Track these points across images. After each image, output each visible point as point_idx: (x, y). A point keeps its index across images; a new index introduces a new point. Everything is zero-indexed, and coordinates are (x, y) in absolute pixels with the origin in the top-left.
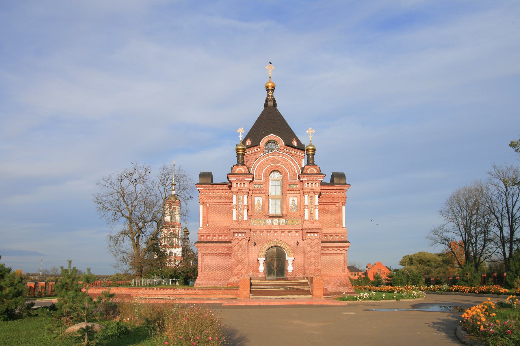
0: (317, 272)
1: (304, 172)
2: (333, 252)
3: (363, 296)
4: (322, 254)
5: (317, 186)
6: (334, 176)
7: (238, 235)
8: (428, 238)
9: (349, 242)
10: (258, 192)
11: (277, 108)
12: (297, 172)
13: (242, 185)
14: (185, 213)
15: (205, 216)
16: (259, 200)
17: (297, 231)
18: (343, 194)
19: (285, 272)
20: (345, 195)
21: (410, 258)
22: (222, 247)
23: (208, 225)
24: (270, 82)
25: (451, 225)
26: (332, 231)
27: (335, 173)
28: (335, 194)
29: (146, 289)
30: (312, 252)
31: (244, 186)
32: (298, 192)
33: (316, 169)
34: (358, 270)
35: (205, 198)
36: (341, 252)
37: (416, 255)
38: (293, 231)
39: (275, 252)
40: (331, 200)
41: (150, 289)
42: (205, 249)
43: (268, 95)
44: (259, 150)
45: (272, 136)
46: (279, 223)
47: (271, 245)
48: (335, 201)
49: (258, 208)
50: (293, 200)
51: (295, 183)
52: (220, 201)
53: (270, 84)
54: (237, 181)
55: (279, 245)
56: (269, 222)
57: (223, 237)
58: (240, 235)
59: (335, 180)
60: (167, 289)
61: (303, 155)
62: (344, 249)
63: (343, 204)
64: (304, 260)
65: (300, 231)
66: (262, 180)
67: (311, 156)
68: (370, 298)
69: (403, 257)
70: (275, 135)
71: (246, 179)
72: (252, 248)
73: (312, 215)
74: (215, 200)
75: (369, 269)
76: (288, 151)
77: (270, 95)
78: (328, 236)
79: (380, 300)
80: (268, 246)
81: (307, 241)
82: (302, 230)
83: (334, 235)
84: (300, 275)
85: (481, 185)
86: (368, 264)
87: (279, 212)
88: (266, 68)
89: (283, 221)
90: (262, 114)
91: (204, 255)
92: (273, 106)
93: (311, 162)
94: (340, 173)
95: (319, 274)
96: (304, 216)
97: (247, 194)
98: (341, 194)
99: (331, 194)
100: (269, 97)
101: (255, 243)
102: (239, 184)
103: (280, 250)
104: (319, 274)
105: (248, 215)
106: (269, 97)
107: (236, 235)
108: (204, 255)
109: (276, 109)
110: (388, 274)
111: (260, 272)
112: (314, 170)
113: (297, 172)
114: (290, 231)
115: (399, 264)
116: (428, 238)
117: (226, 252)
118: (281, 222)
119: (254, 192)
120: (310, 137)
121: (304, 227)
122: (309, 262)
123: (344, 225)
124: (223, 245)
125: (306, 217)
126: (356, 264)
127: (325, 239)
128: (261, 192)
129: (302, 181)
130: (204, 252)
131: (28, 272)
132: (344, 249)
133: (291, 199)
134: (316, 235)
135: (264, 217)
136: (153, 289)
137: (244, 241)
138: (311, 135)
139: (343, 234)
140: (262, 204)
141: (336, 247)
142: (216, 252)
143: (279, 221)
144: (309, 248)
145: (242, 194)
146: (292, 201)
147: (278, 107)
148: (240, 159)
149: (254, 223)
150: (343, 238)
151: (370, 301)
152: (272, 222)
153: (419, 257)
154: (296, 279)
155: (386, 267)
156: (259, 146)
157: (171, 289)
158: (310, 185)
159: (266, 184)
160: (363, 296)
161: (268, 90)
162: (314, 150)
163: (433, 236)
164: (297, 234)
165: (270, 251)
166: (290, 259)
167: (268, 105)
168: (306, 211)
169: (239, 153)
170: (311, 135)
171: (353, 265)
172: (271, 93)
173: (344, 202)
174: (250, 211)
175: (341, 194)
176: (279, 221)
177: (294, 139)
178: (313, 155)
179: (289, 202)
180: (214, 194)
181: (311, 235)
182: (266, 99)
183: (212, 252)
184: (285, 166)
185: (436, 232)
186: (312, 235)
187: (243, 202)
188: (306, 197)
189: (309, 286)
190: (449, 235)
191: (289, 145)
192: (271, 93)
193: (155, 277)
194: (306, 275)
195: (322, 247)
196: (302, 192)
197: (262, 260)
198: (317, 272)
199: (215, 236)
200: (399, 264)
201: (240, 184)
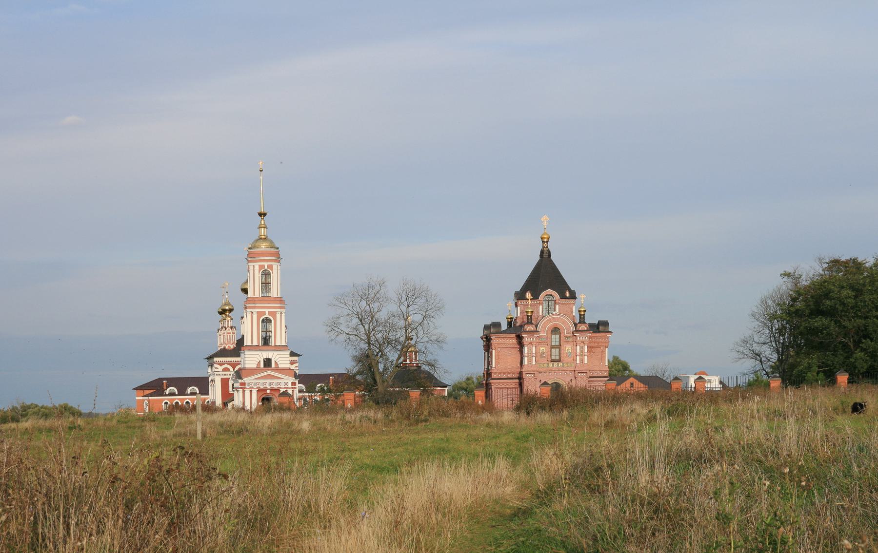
1: (577, 329)
15: (497, 358)
17: (571, 371)
22: (510, 383)
26: (597, 368)
31: (533, 340)
32: (572, 343)
43: (544, 247)
44: (538, 302)
45: (549, 291)
46: (558, 366)
51: (570, 337)
52: (509, 346)
53: (545, 236)
55: (557, 381)
56: (551, 365)
63: (606, 347)
73: (582, 360)
81: (578, 379)
82: (574, 371)
85: (394, 414)
87: (557, 358)
89: (560, 364)
120: (582, 301)
121: (577, 369)
124: (511, 381)
127: (591, 374)
131: (627, 361)
134: (585, 374)
135: (547, 362)
137: (533, 380)
141: (600, 381)
145: (531, 346)
147: (552, 258)
152: (553, 365)
161: (543, 242)
163: (741, 349)
168: (578, 357)
172: (546, 245)
174: (537, 359)
185: (745, 342)
186: (582, 374)
187: (532, 351)
188: (578, 347)
191: (563, 297)
192: (546, 245)
196: (575, 343)
199: (504, 374)
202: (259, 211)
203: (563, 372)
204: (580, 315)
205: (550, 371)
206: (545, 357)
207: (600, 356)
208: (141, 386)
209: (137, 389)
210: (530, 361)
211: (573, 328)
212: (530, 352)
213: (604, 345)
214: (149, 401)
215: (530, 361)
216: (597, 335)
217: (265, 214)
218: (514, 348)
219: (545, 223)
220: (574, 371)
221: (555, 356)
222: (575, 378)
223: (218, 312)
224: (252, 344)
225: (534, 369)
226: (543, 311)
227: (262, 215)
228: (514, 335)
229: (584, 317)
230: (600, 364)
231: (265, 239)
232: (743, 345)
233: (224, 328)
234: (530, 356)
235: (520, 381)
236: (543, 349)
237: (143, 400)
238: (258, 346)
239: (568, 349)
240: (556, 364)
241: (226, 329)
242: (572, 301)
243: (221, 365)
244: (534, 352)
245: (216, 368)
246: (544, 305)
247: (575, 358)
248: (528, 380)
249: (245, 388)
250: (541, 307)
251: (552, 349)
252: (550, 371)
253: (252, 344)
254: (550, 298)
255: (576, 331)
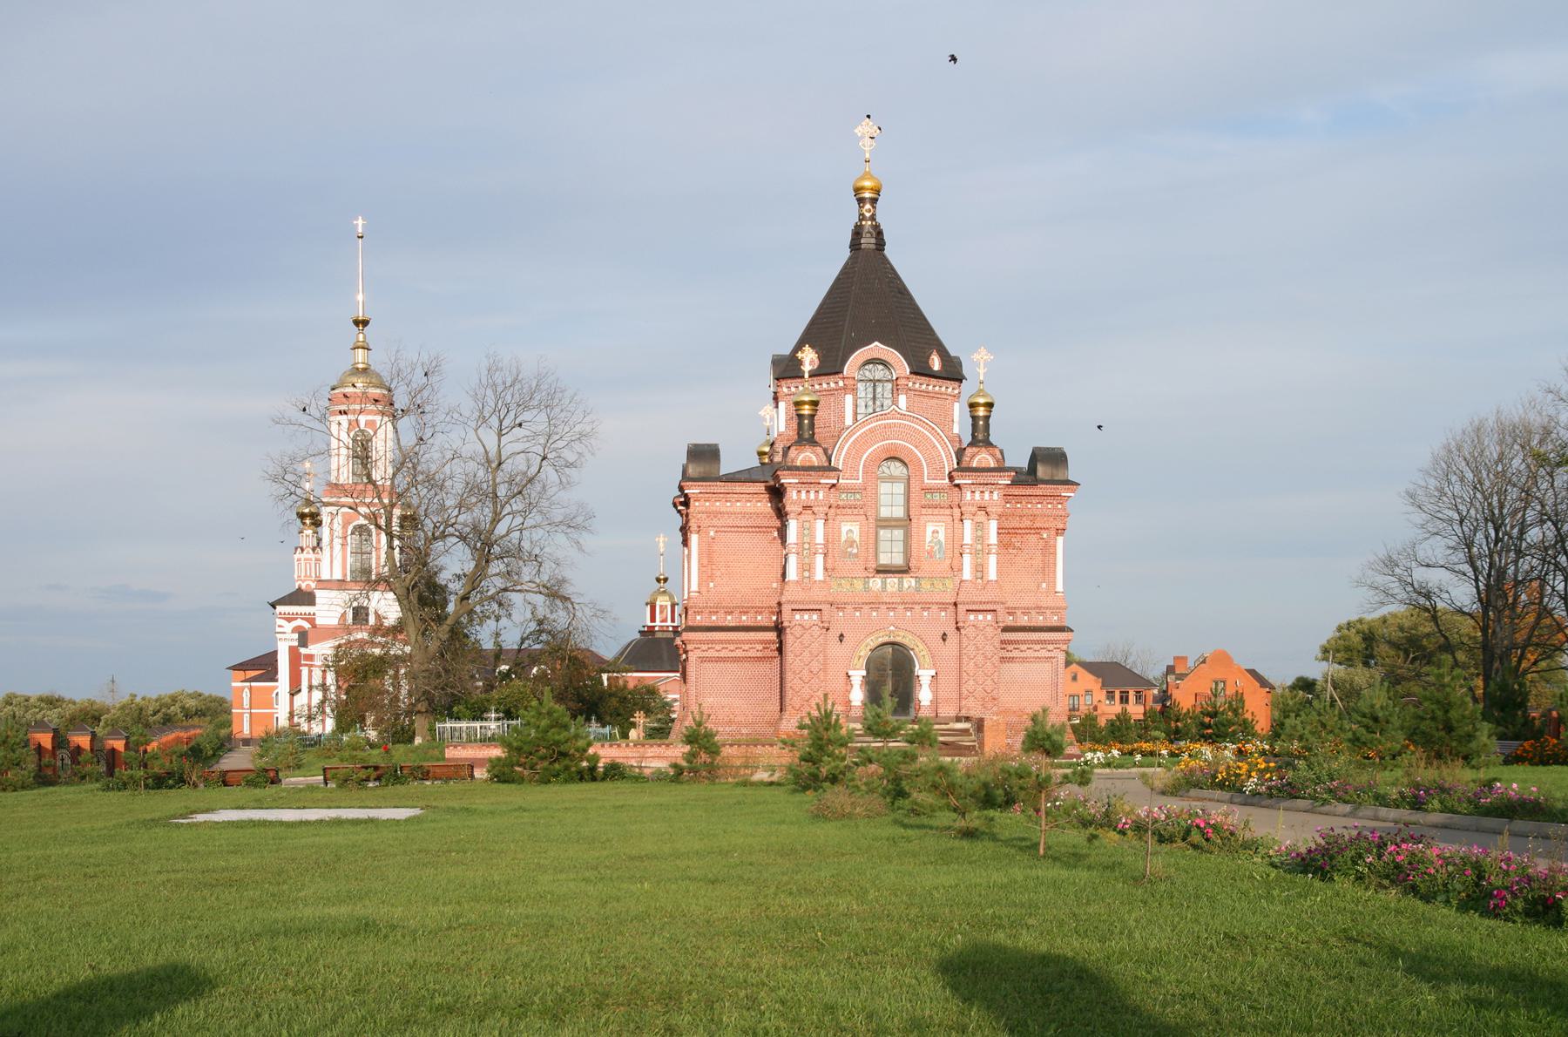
0: (990, 705)
1: (964, 465)
2: (1029, 653)
3: (1093, 758)
4: (1003, 660)
5: (995, 496)
6: (1037, 456)
7: (802, 616)
8: (1359, 583)
9: (1072, 631)
10: (849, 511)
11: (886, 252)
12: (946, 463)
13: (812, 496)
14: (579, 520)
15: (705, 561)
16: (851, 530)
17: (943, 606)
18: (1060, 506)
19: (912, 705)
20: (1065, 509)
21: (1363, 633)
23: (711, 585)
24: (867, 176)
25: (1439, 548)
26: (1028, 601)
27: (1040, 449)
28: (1039, 506)
29: (603, 746)
30: (980, 658)
31: (816, 498)
32: (948, 511)
33: (993, 455)
34: (1141, 682)
35: (704, 516)
36: (1049, 654)
37: (1391, 621)
38: (934, 607)
39: (890, 656)
40: (1028, 523)
41: (611, 746)
42: (704, 647)
43: (862, 217)
44: (841, 384)
45: (876, 349)
47: (881, 640)
48: (1038, 525)
49: (849, 550)
50: (934, 531)
51: (940, 490)
53: (867, 184)
54: (799, 485)
55: (898, 639)
56: (876, 583)
57: (750, 615)
58: (806, 617)
59: (1041, 471)
60: (652, 746)
61: (956, 391)
62: (1058, 646)
63: (1060, 531)
64: (960, 677)
65: (952, 608)
66: (860, 481)
67: (981, 423)
68: (1108, 765)
69: (1340, 629)
70: (884, 344)
71: (822, 481)
72: (835, 649)
73: (980, 569)
74: (730, 522)
75: (1181, 677)
76: (917, 386)
77: (868, 215)
78: (1019, 613)
79: (1127, 768)
80: (873, 642)
82: (955, 604)
83: (1033, 612)
84: (948, 711)
86: (1176, 658)
87: (898, 560)
88: (856, 131)
89: (909, 582)
90: (846, 273)
91: (703, 660)
92: (877, 249)
93: (980, 437)
94: (1053, 449)
95: (995, 709)
96: (961, 570)
97: (823, 516)
98: (1055, 508)
99: (1029, 506)
100: (864, 223)
101: (842, 635)
102: (804, 493)
103: (902, 652)
104: (995, 709)
105: (826, 569)
106: (864, 223)
107: (798, 617)
108: (703, 660)
109: (885, 260)
110: (1205, 706)
111: (853, 704)
112: (990, 458)
113: (946, 463)
114: (926, 606)
115: (1316, 659)
116: (1359, 583)
117: (759, 654)
118: (906, 585)
119: (838, 511)
120: (982, 371)
122: (971, 682)
123: (1060, 587)
125: (967, 574)
126: (1131, 654)
127: (1010, 620)
128: (856, 511)
129: (958, 486)
130: (705, 654)
132: (1058, 646)
133: (930, 528)
135: (866, 574)
136: (619, 746)
137: (816, 631)
138: (982, 365)
139: (1056, 610)
140: (858, 540)
141: (1033, 642)
142: (732, 654)
143: (901, 583)
144: (971, 648)
145: (811, 517)
146: (933, 532)
147: (888, 252)
148: (806, 427)
149: (842, 589)
150: (1056, 618)
151: (1107, 770)
152: (884, 584)
153: (1401, 629)
154: (938, 720)
155: (1248, 671)
156: (841, 376)
157: (660, 746)
158: (977, 495)
159: (868, 491)
160: (1093, 758)
161: (861, 201)
162: (990, 405)
163: (1380, 580)
164: (943, 614)
165: (877, 653)
166: (924, 674)
167: (863, 246)
168: (967, 559)
169: (802, 412)
170: (982, 365)
171: (1119, 659)
173: (1061, 526)
175: (1055, 508)
176: (901, 583)
177: (935, 352)
178: (987, 418)
179: (924, 536)
180: (728, 504)
181: (976, 618)
182: (856, 226)
183: (722, 654)
184: (916, 447)
185: (1390, 563)
187: (813, 536)
188: (968, 524)
189: (973, 738)
190: (1434, 578)
191: (921, 370)
193: (493, 715)
194: (964, 713)
195: (1003, 642)
196: (957, 511)
197: (858, 675)
198: (990, 705)
200: (1316, 659)
201: (808, 492)
202: (354, 316)
203: (917, 607)
204: (974, 418)
205: (875, 605)
206: (856, 555)
207: (1038, 561)
208: (241, 664)
209: (234, 668)
210: (805, 567)
211: (950, 463)
212: (806, 539)
213: (1053, 524)
214: (251, 688)
215: (805, 567)
216: (1029, 491)
217: (365, 323)
218: (759, 529)
219: (867, 146)
220: (955, 604)
221: (891, 554)
222: (958, 629)
223: (298, 514)
224: (331, 575)
225: (818, 594)
226: (855, 414)
227: (362, 323)
228: (760, 488)
229: (987, 426)
230: (1039, 586)
231: (365, 370)
232: (1386, 571)
233: (299, 550)
234: (805, 550)
235: (779, 636)
236: (850, 529)
237: (243, 688)
238: (343, 581)
239: (934, 531)
240: (892, 581)
241: (302, 550)
242: (949, 388)
243: (289, 620)
244: (820, 538)
245: (280, 626)
246: (861, 394)
247: (955, 563)
248: (798, 631)
249: (312, 666)
250: (849, 399)
251: (882, 532)
252: (875, 605)
253: (331, 575)
254: (879, 372)
255: (962, 469)
